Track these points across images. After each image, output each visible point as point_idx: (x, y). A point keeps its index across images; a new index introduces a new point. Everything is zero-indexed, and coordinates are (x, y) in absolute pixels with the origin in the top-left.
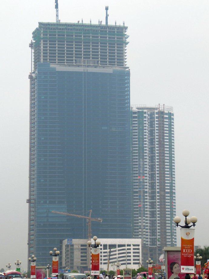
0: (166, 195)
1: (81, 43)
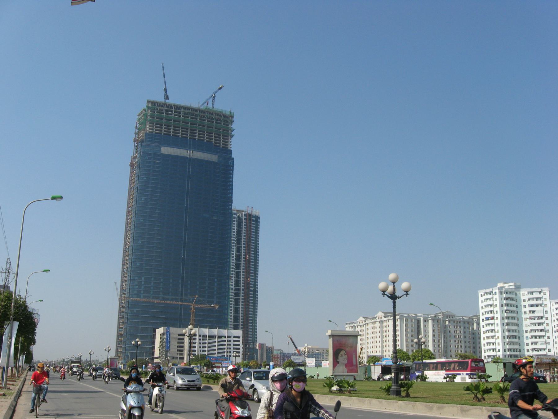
0: (251, 293)
1: (188, 129)
